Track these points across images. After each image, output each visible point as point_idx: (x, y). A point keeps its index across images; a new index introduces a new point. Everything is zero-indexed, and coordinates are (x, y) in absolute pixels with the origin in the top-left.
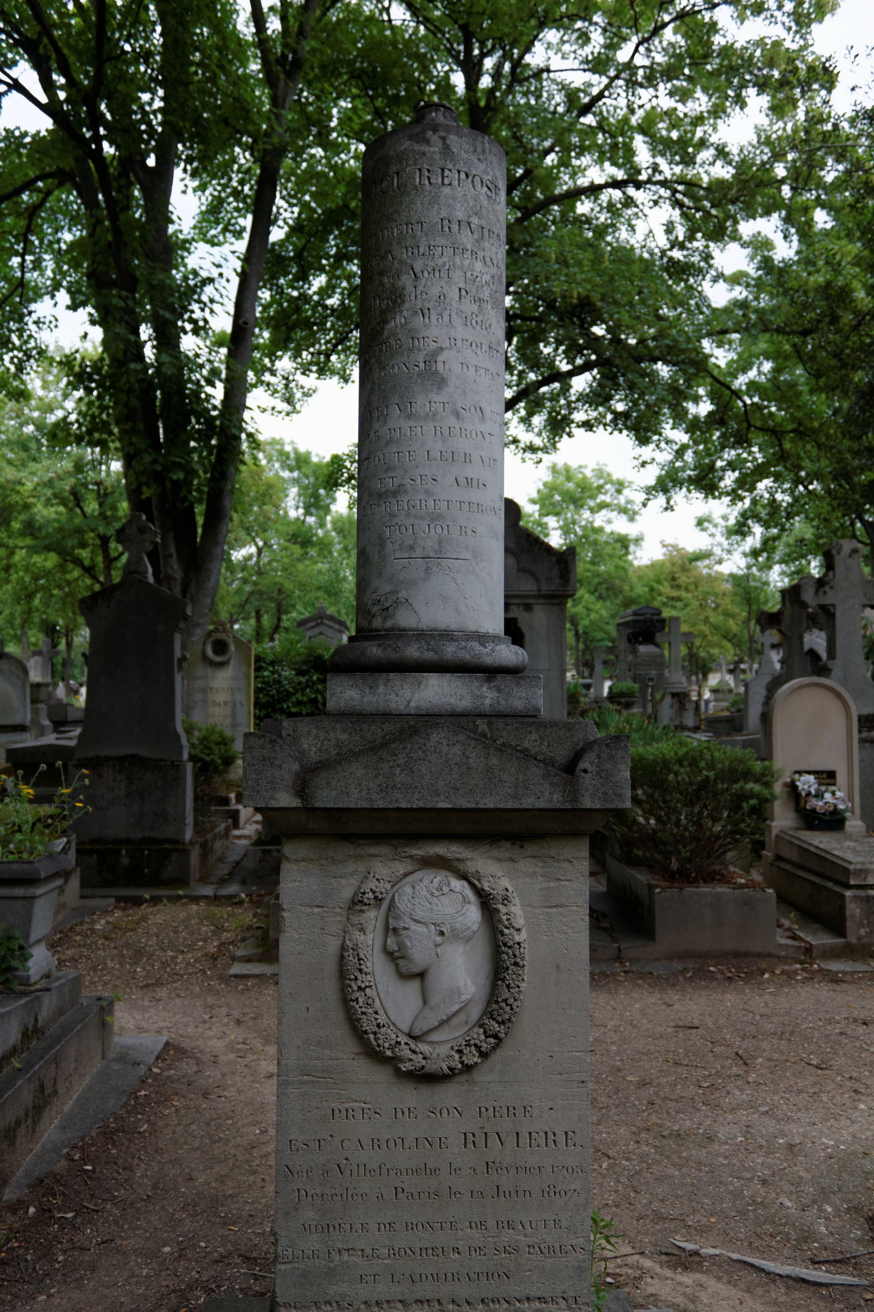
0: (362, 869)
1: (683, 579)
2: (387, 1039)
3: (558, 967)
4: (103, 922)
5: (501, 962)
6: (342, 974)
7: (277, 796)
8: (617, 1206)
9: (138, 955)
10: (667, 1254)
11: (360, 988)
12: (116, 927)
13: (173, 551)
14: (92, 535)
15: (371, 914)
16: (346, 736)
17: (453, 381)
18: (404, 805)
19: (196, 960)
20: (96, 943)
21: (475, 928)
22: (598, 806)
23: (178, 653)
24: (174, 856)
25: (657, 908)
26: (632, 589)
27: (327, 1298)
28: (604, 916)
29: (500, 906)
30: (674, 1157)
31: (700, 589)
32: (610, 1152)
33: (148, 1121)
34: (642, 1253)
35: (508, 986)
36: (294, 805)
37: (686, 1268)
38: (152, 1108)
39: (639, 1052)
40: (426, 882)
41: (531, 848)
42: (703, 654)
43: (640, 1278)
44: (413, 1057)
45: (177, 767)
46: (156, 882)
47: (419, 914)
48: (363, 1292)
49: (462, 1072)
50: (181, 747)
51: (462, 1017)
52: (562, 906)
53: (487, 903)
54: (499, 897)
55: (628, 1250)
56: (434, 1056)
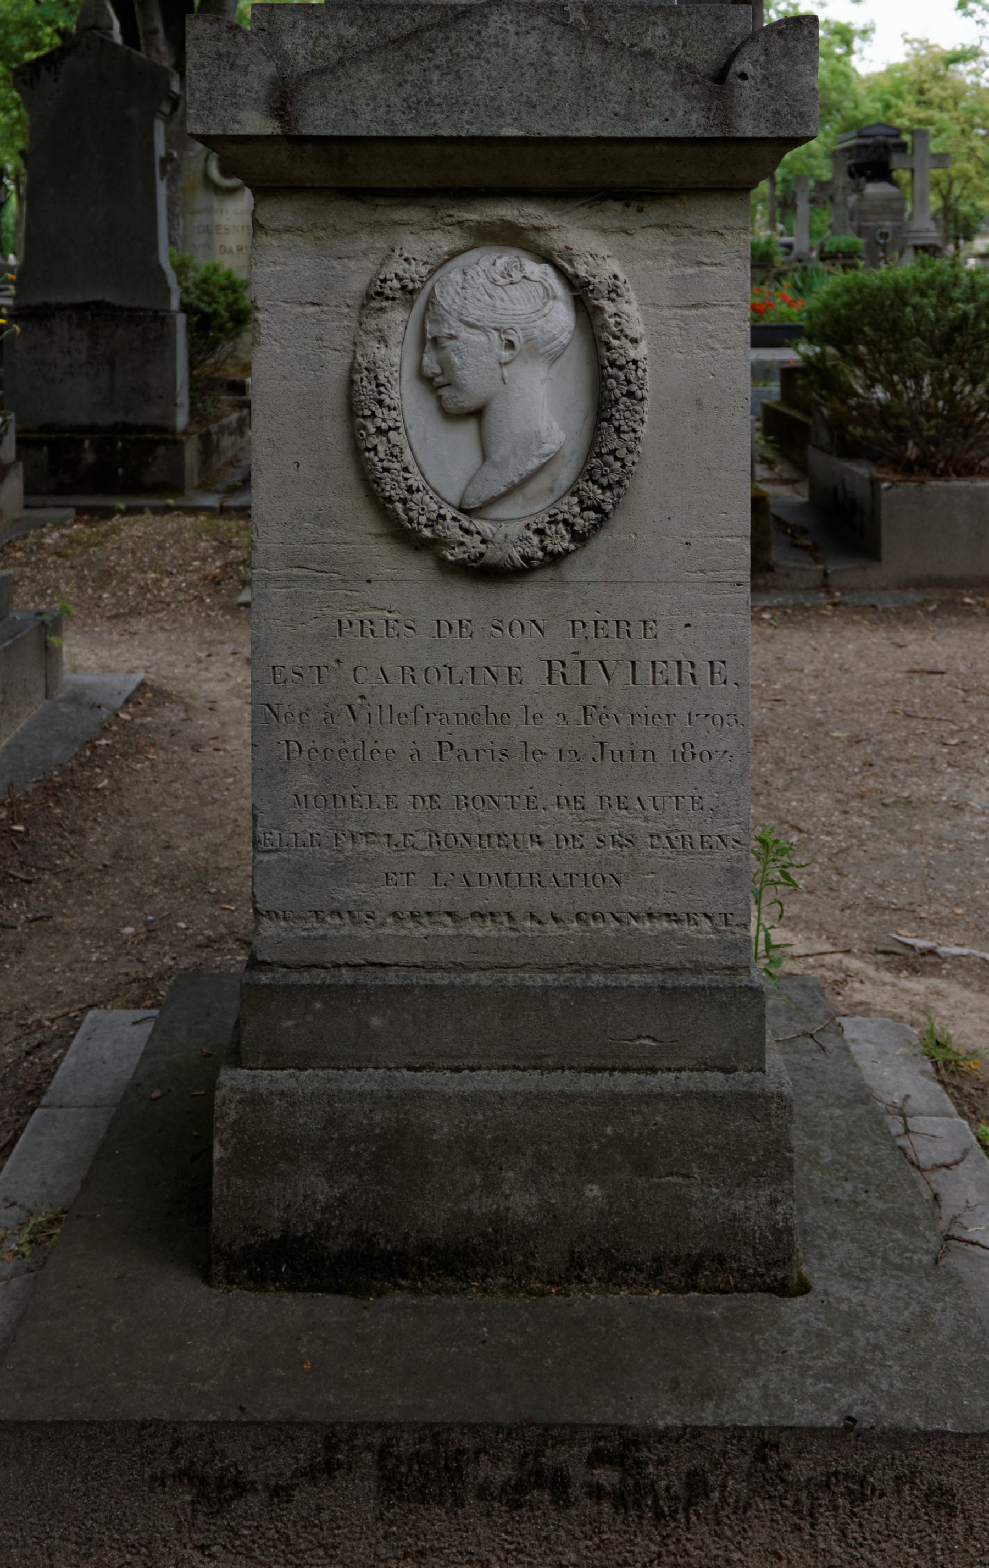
0: (381, 243)
1: (935, 92)
2: (422, 509)
3: (699, 403)
4: (56, 535)
5: (608, 392)
6: (352, 410)
7: (242, 116)
8: (811, 892)
9: (105, 576)
10: (885, 953)
11: (379, 431)
12: (73, 541)
13: (159, 24)
14: (49, 30)
15: (397, 315)
16: (354, 30)
18: (446, 132)
19: (190, 585)
20: (44, 560)
21: (565, 338)
22: (765, 133)
23: (160, 150)
24: (161, 450)
25: (884, 513)
26: (856, 107)
27: (336, 905)
28: (804, 531)
29: (604, 303)
30: (902, 832)
31: (962, 104)
32: (802, 825)
33: (110, 777)
34: (847, 952)
35: (618, 430)
36: (269, 131)
37: (915, 971)
38: (116, 761)
39: (851, 702)
40: (485, 264)
41: (656, 213)
42: (964, 208)
43: (843, 983)
44: (466, 539)
45: (162, 318)
46: (134, 487)
47: (473, 314)
48: (390, 897)
49: (543, 565)
50: (168, 290)
51: (543, 481)
52: (706, 305)
53: (582, 296)
54: (604, 288)
55: (827, 947)
56: (499, 537)
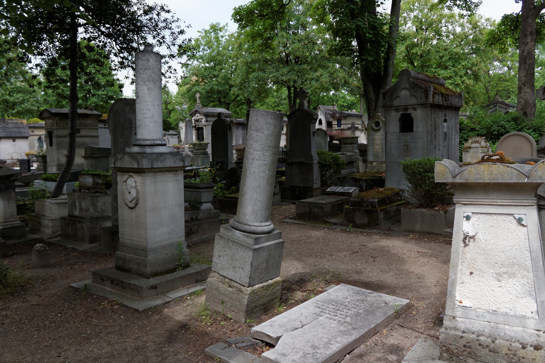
13: (371, 89)
17: (140, 97)
24: (309, 192)
45: (310, 166)
